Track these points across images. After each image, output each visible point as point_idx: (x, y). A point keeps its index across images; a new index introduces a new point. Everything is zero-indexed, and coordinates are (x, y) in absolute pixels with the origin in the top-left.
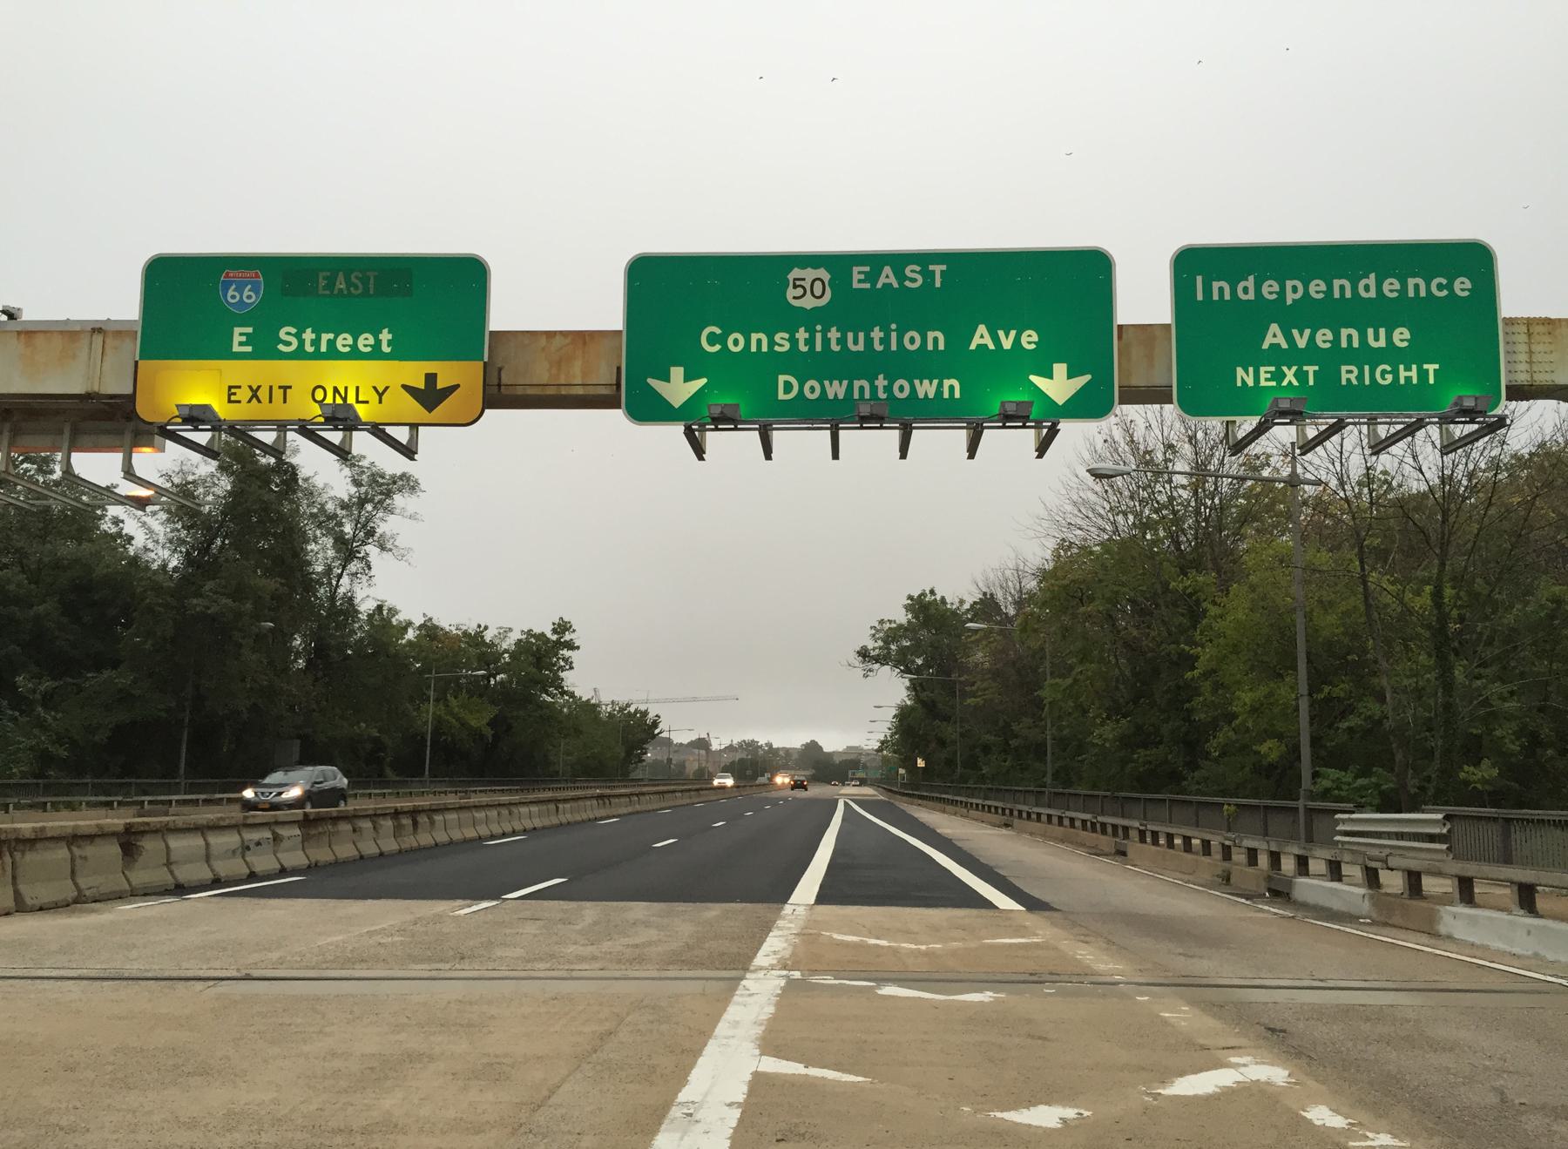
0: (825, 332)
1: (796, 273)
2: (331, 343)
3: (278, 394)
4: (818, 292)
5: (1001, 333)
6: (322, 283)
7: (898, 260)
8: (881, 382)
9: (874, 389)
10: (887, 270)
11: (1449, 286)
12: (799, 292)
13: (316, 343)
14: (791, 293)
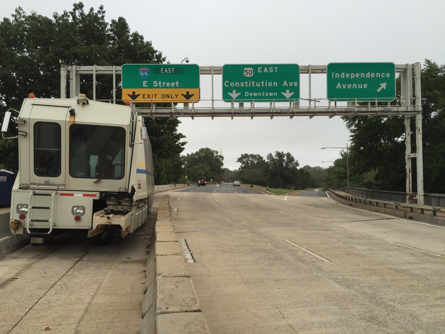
0: (251, 82)
1: (246, 69)
2: (165, 85)
3: (154, 96)
4: (250, 73)
5: (343, 85)
6: (162, 70)
7: (268, 66)
8: (263, 93)
9: (262, 94)
10: (266, 68)
11: (385, 75)
12: (247, 73)
13: (162, 84)
14: (245, 73)
